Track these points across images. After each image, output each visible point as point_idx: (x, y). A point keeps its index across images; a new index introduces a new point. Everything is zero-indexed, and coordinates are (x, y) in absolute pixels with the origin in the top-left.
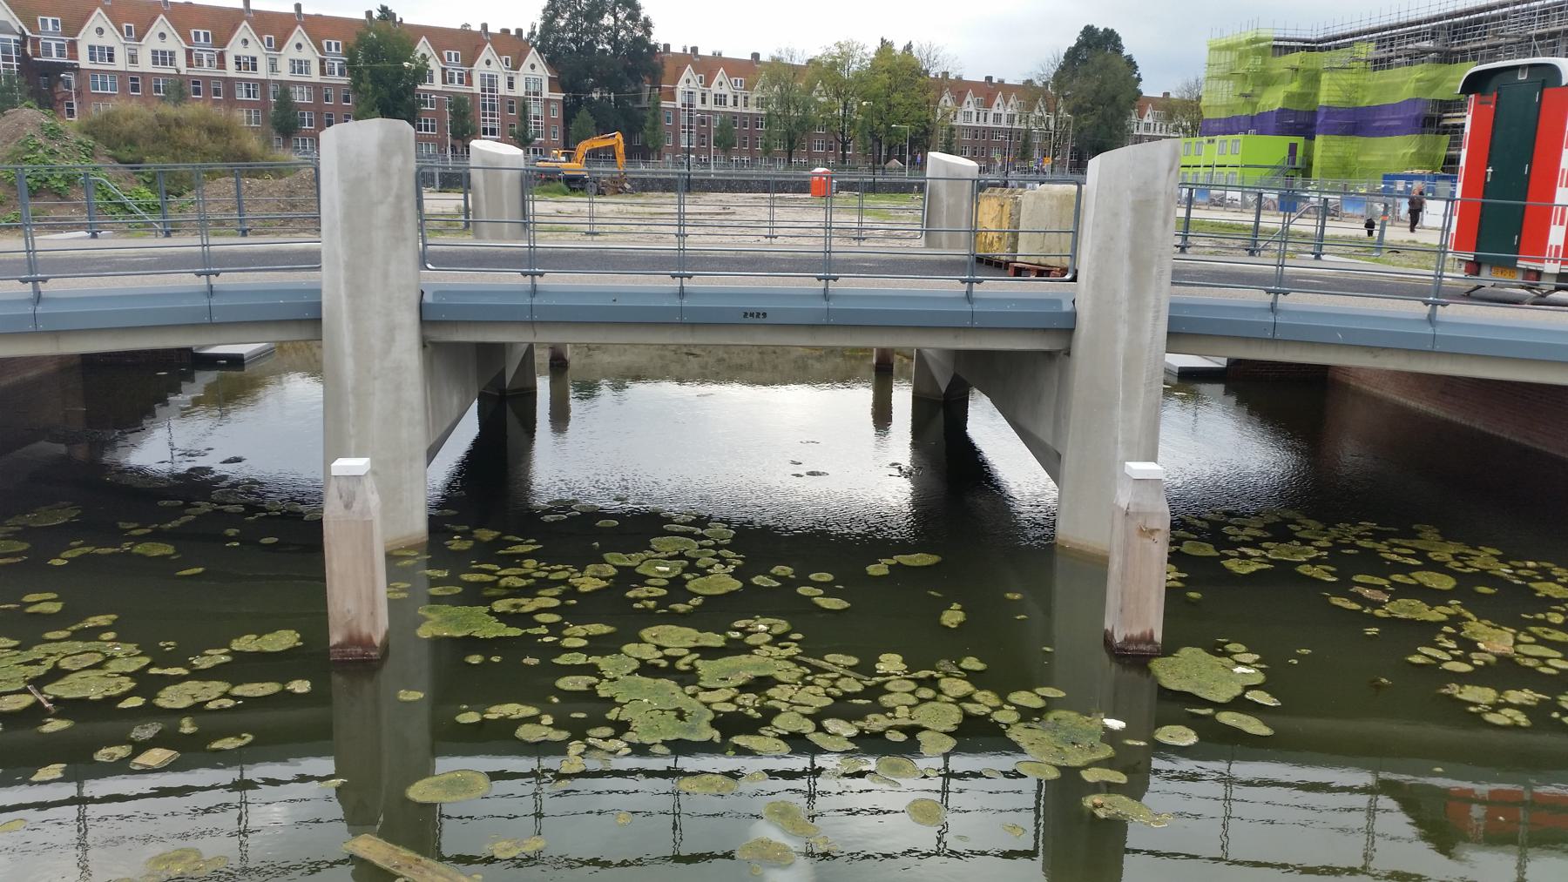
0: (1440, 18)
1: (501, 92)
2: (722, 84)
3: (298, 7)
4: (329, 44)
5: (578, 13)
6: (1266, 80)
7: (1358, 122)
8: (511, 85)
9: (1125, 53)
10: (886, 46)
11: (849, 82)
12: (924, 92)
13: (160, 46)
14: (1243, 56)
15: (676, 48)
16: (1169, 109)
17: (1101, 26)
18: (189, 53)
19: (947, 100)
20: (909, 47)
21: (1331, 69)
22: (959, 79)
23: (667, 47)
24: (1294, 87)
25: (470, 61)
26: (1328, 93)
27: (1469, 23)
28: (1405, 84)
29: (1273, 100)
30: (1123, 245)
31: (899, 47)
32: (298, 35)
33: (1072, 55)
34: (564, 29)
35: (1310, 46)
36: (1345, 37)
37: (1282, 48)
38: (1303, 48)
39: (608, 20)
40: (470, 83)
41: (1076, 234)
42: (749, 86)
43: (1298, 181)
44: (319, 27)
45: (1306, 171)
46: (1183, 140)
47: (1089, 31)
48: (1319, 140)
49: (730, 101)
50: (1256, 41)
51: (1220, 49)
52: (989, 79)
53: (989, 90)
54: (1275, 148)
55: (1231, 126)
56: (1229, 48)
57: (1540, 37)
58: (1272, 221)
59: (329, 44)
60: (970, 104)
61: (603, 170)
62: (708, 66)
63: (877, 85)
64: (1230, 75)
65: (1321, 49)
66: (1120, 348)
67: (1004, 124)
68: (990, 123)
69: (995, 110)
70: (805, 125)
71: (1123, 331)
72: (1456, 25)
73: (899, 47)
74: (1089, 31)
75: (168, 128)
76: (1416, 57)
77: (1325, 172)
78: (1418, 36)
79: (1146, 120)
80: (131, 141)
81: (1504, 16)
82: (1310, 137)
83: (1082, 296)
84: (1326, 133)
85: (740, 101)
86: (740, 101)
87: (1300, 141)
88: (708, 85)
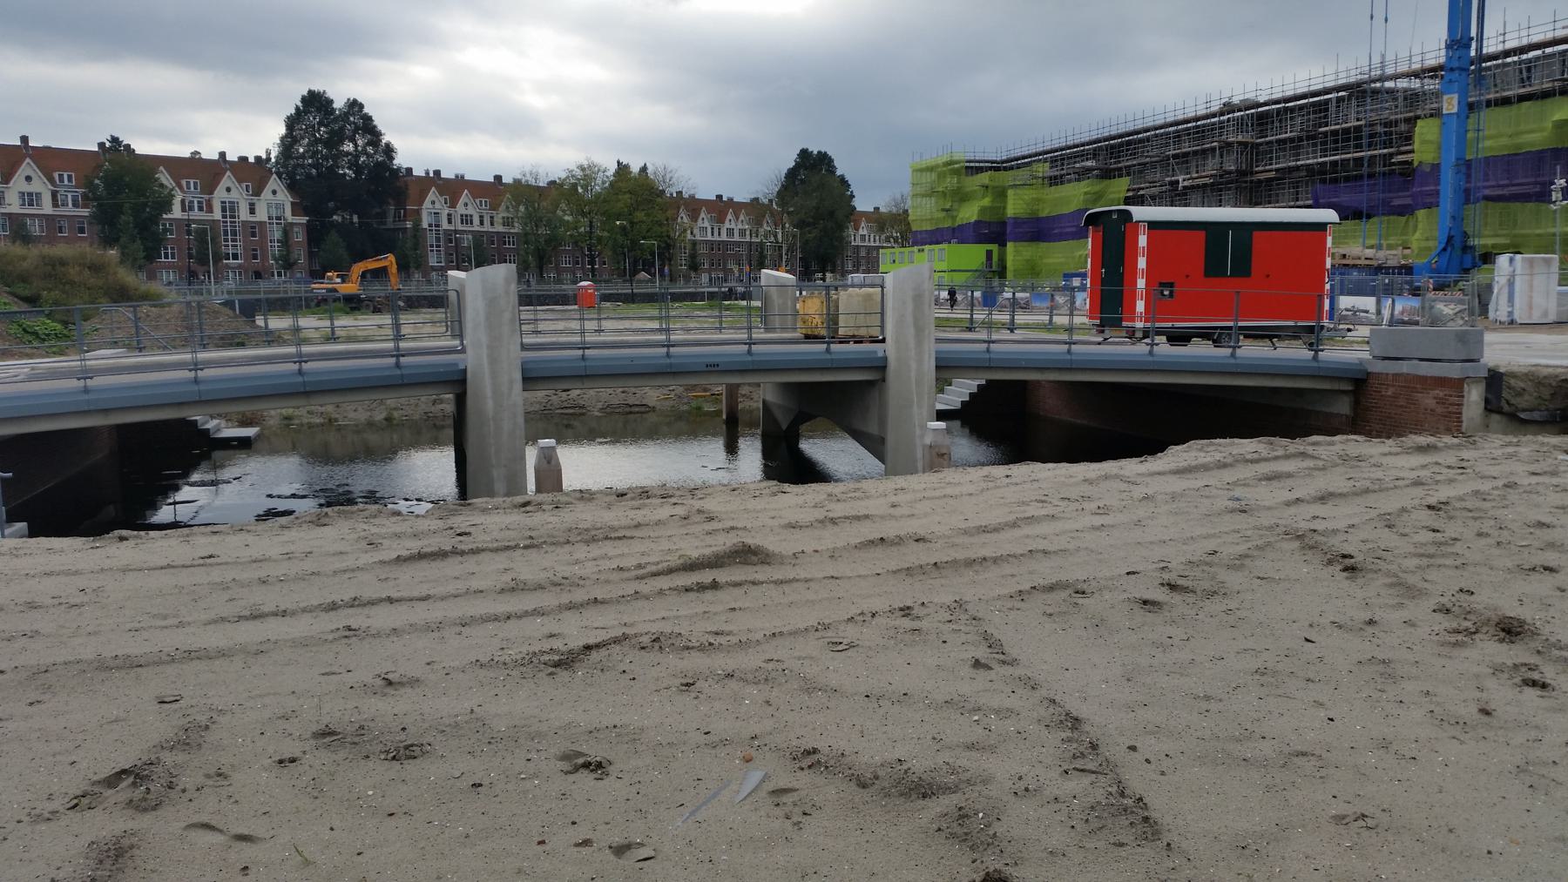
0: (1098, 141)
1: (243, 218)
2: (466, 205)
3: (24, 139)
4: (61, 176)
5: (318, 141)
6: (961, 197)
7: (1038, 230)
8: (252, 211)
9: (838, 173)
10: (622, 169)
11: (590, 202)
12: (663, 209)
13: (27, 188)
14: (941, 176)
15: (418, 172)
16: (880, 221)
17: (814, 149)
18: (54, 195)
19: (684, 218)
20: (644, 169)
21: (1015, 186)
22: (692, 197)
23: (409, 170)
24: (986, 202)
25: (210, 188)
26: (1015, 206)
27: (1121, 145)
28: (1073, 197)
29: (969, 213)
30: (910, 319)
31: (635, 169)
32: (28, 167)
33: (792, 174)
34: (303, 156)
35: (997, 167)
36: (1024, 157)
37: (974, 169)
38: (990, 168)
39: (348, 147)
40: (210, 210)
41: (882, 314)
42: (494, 207)
43: (996, 282)
44: (50, 159)
45: (1002, 273)
46: (897, 250)
47: (804, 154)
48: (1010, 246)
49: (476, 221)
50: (951, 163)
51: (921, 170)
52: (719, 197)
53: (720, 207)
54: (974, 255)
55: (936, 237)
56: (930, 169)
57: (1175, 156)
58: (980, 315)
59: (61, 176)
60: (704, 221)
61: (377, 290)
62: (454, 188)
63: (620, 205)
64: (932, 193)
65: (1005, 169)
66: (913, 374)
67: (737, 238)
68: (724, 237)
69: (727, 225)
70: (554, 242)
71: (914, 365)
72: (1112, 147)
73: (635, 169)
74: (804, 154)
75: (53, 266)
76: (1083, 174)
77: (1017, 273)
78: (1083, 156)
79: (861, 232)
80: (24, 279)
81: (1148, 139)
82: (1003, 244)
83: (890, 349)
84: (1015, 240)
85: (487, 221)
86: (487, 221)
87: (994, 247)
88: (453, 206)
